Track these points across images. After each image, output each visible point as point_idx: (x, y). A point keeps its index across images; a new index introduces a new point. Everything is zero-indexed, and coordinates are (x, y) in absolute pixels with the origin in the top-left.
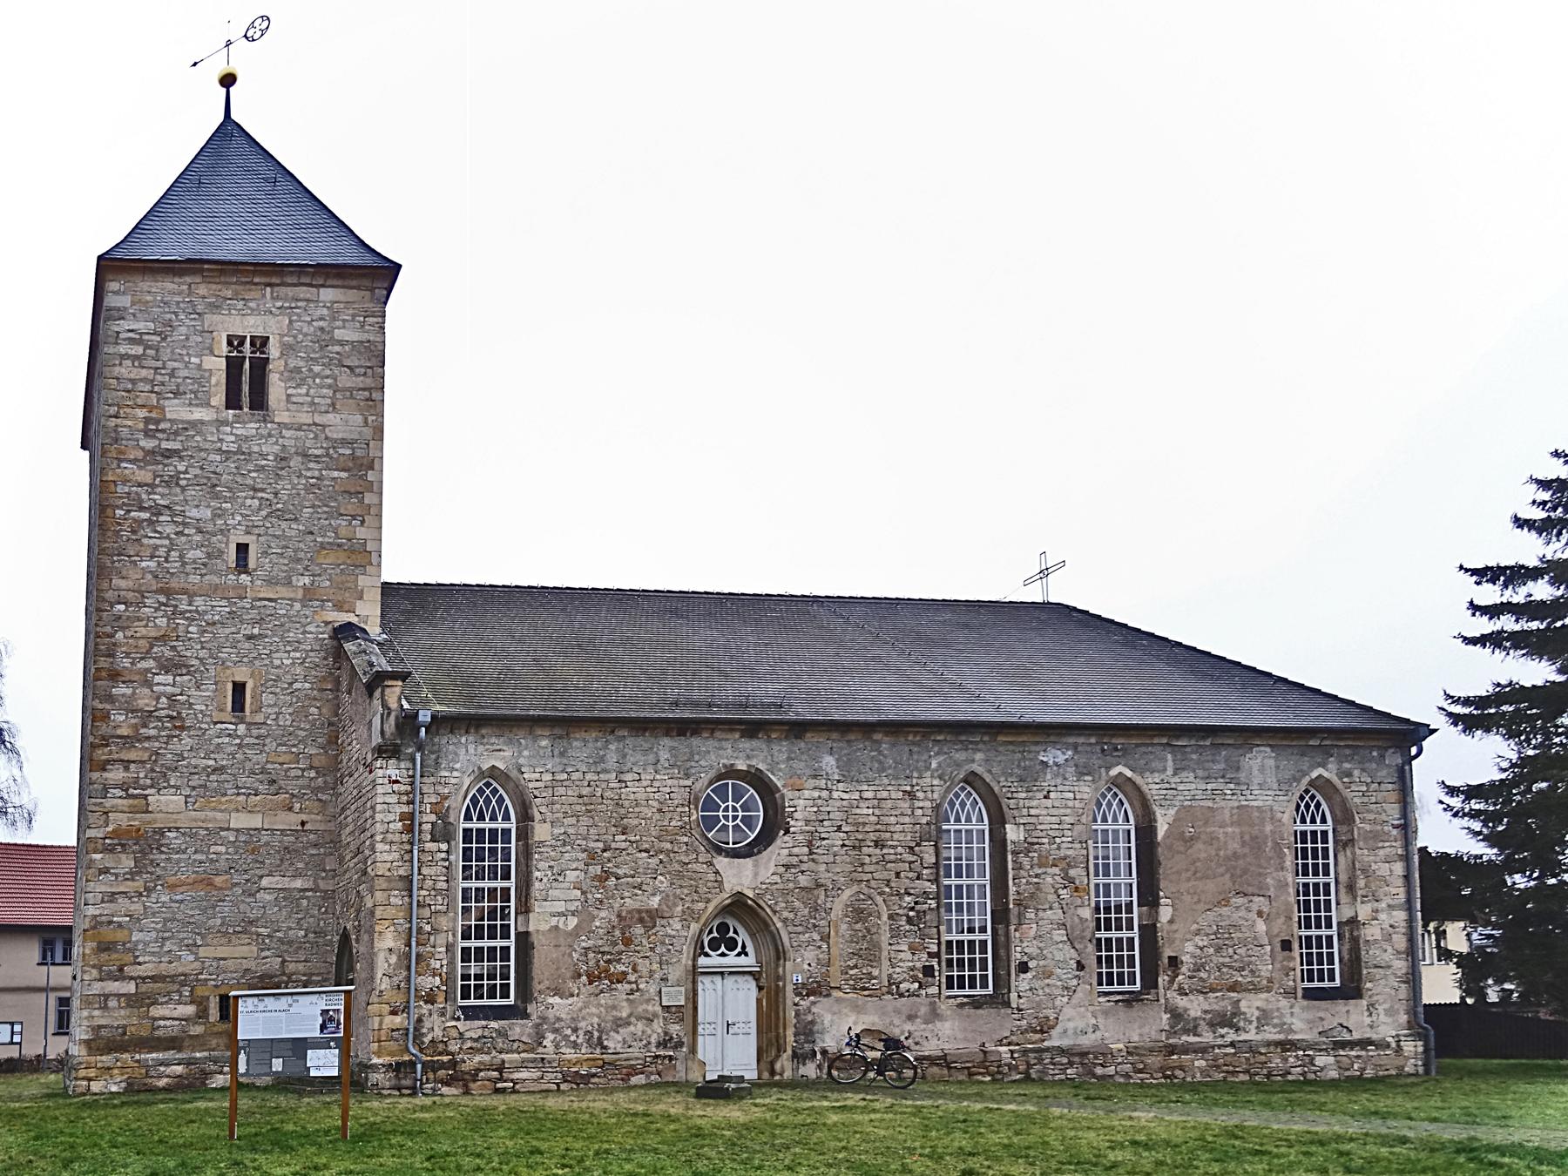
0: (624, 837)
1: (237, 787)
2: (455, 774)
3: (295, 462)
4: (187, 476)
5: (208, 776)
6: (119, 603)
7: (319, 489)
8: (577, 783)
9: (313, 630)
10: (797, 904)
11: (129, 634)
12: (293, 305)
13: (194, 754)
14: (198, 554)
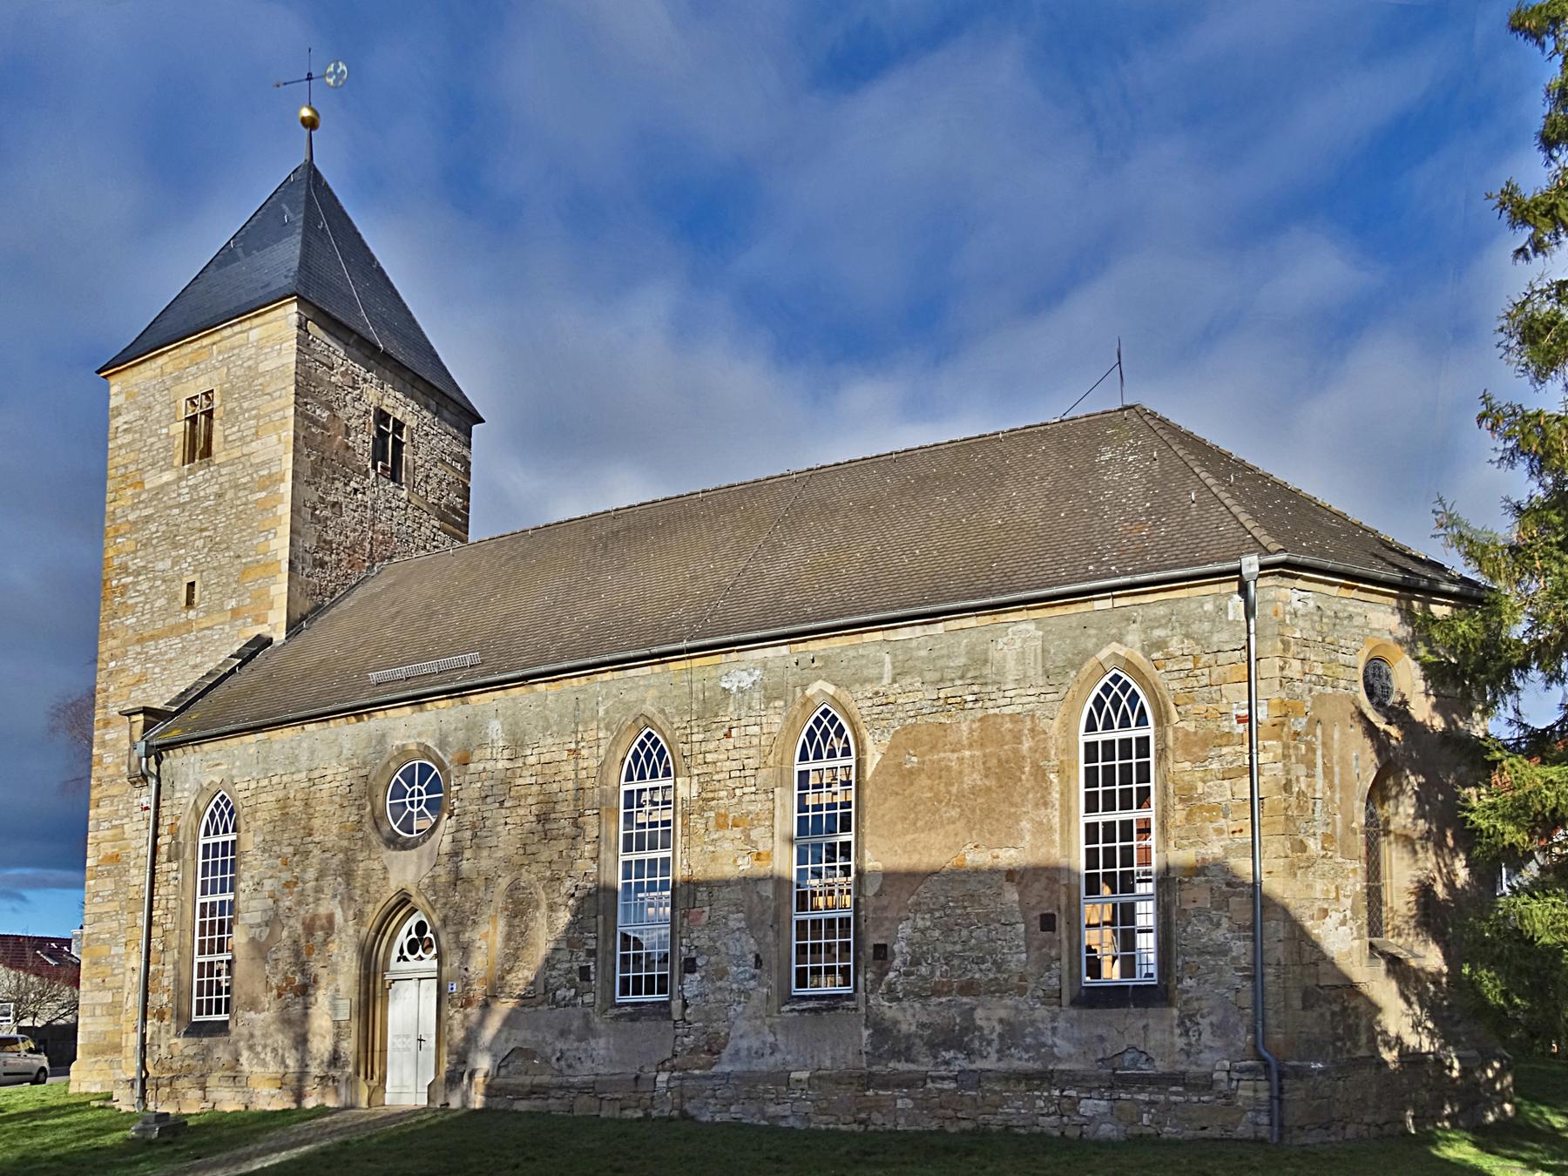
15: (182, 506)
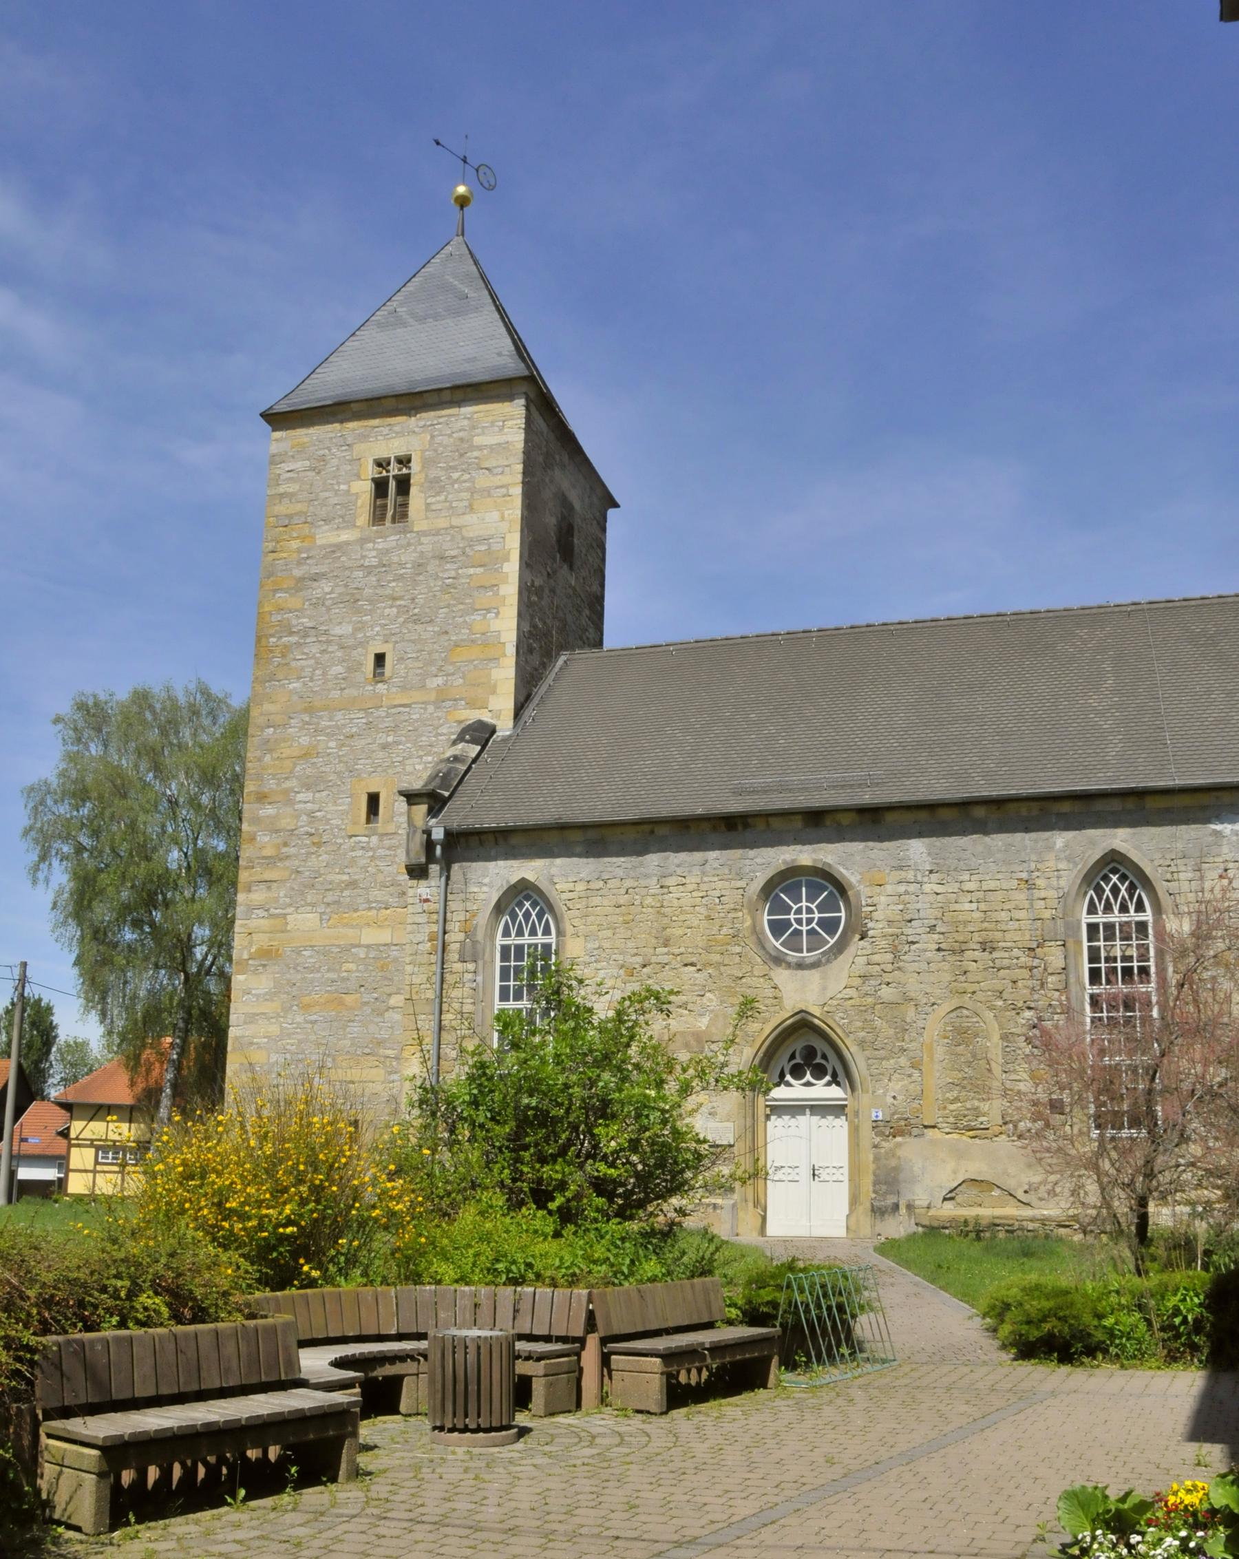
0: (666, 950)
1: (369, 902)
2: (485, 889)
3: (432, 567)
4: (333, 596)
5: (342, 892)
6: (269, 727)
7: (455, 588)
8: (615, 891)
9: (445, 731)
10: (878, 1022)
11: (275, 755)
12: (435, 422)
13: (330, 870)
14: (340, 669)
15: (369, 570)
